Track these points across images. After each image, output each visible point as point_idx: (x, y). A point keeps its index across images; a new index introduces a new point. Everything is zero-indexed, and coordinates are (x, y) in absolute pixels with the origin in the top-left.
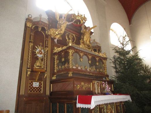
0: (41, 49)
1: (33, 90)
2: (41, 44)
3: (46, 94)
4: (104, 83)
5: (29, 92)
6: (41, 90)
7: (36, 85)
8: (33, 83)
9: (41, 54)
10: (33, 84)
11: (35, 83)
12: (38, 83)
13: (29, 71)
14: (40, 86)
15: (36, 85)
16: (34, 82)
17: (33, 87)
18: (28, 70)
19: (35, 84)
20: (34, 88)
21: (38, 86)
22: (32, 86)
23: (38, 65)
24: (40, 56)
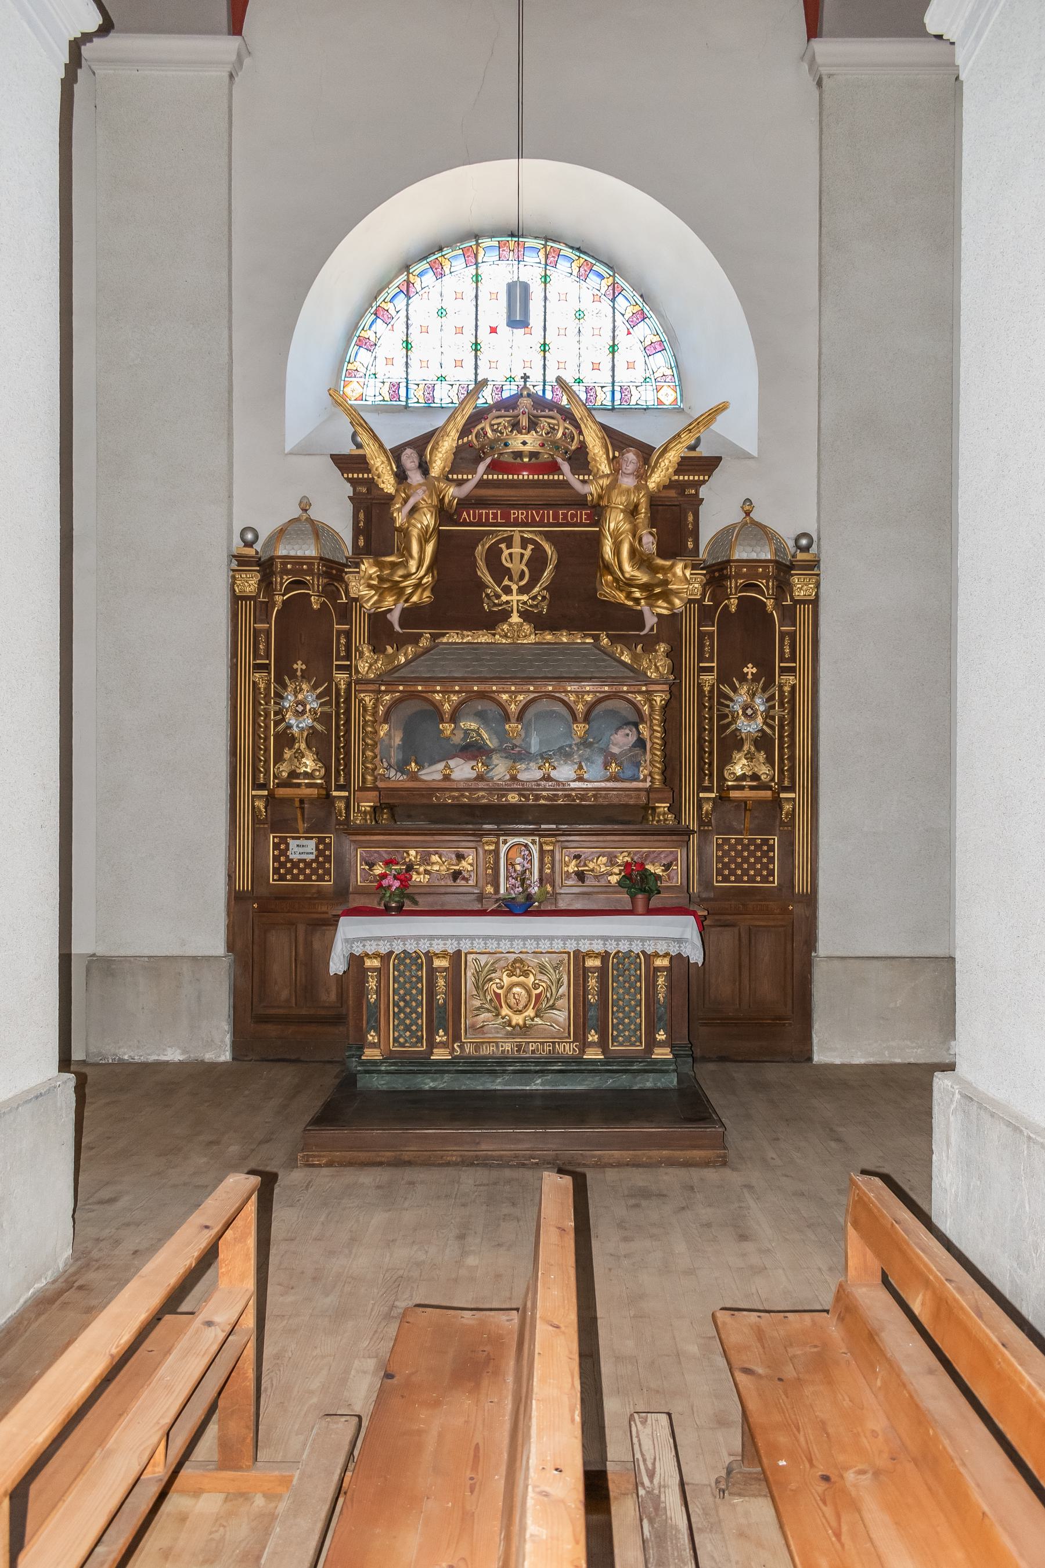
0: (753, 695)
1: (289, 871)
2: (750, 670)
3: (793, 887)
4: (650, 701)
5: (717, 882)
6: (771, 873)
7: (301, 850)
8: (287, 845)
9: (751, 718)
10: (287, 848)
11: (298, 842)
12: (311, 845)
13: (709, 799)
14: (320, 853)
15: (301, 850)
16: (293, 838)
17: (316, 860)
18: (701, 795)
19: (296, 849)
20: (295, 864)
21: (313, 857)
22: (313, 861)
23: (739, 773)
24: (748, 727)
